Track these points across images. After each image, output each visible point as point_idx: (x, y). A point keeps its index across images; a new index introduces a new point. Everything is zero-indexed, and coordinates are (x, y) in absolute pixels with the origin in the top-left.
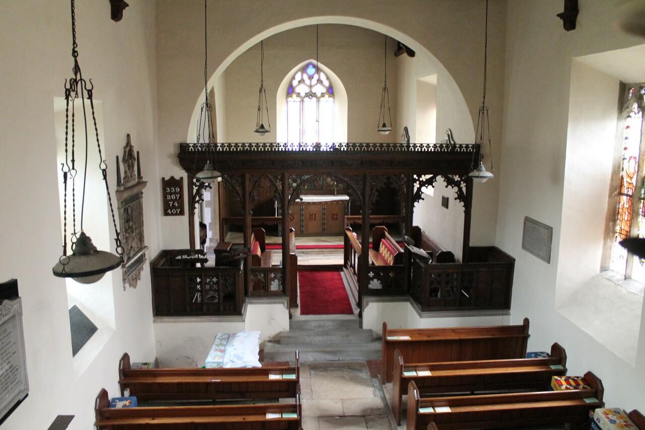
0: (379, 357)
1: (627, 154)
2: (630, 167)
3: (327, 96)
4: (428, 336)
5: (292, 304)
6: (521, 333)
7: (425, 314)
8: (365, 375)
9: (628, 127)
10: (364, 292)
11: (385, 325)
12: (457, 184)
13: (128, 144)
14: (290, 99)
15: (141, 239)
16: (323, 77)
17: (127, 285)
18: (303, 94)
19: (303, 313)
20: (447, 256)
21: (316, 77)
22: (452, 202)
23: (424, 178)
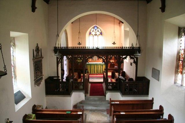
0: (109, 108)
1: (181, 48)
2: (182, 52)
3: (100, 35)
4: (123, 102)
5: (86, 93)
6: (151, 102)
7: (123, 96)
8: (105, 113)
9: (181, 40)
10: (108, 89)
11: (110, 99)
12: (133, 58)
13: (37, 46)
14: (90, 36)
15: (42, 73)
16: (99, 30)
17: (36, 86)
18: (93, 35)
19: (90, 95)
20: (131, 79)
21: (97, 30)
22: (133, 64)
23: (124, 57)
